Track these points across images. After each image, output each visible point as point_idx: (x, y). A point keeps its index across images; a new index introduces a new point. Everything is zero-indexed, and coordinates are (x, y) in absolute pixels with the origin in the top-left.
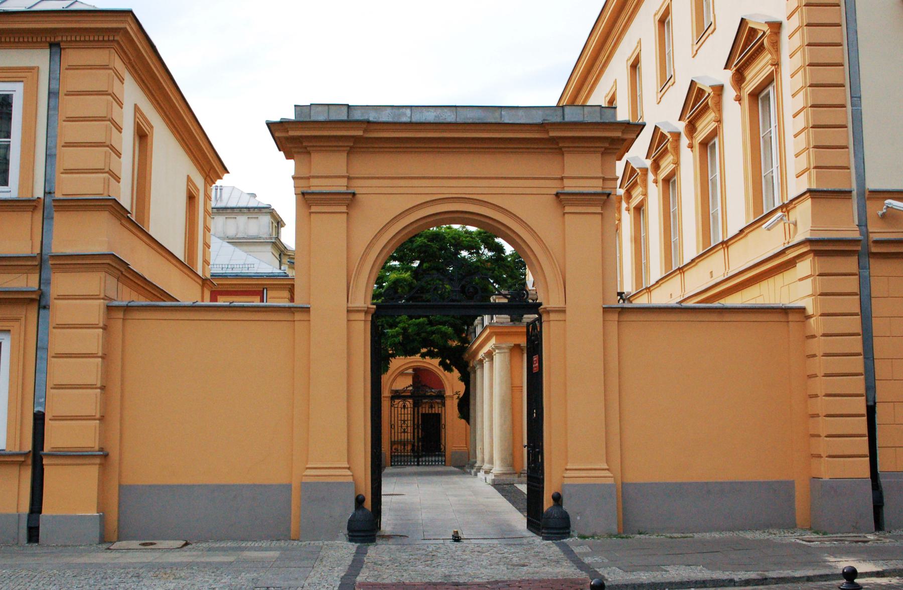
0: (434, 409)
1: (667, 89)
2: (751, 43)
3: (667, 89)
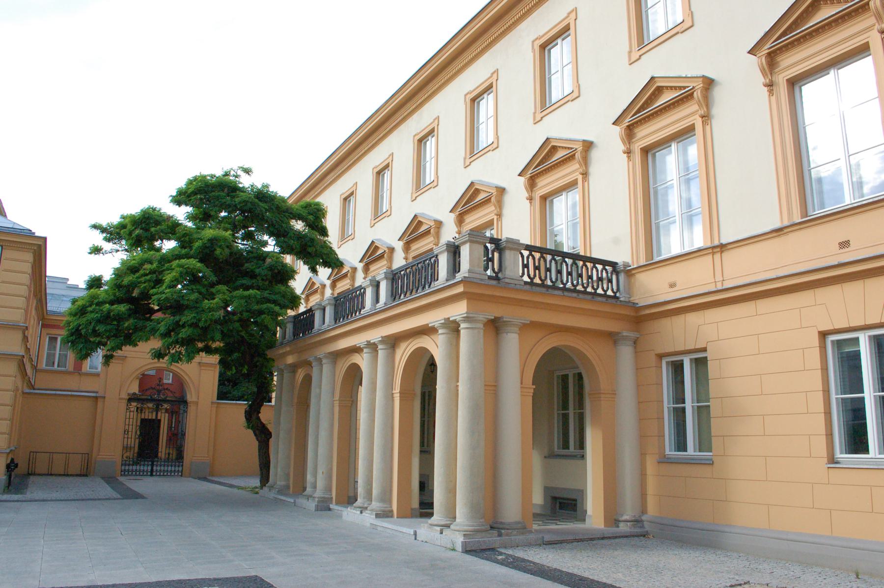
0: (143, 414)
1: (380, 220)
2: (791, 33)
3: (380, 220)
